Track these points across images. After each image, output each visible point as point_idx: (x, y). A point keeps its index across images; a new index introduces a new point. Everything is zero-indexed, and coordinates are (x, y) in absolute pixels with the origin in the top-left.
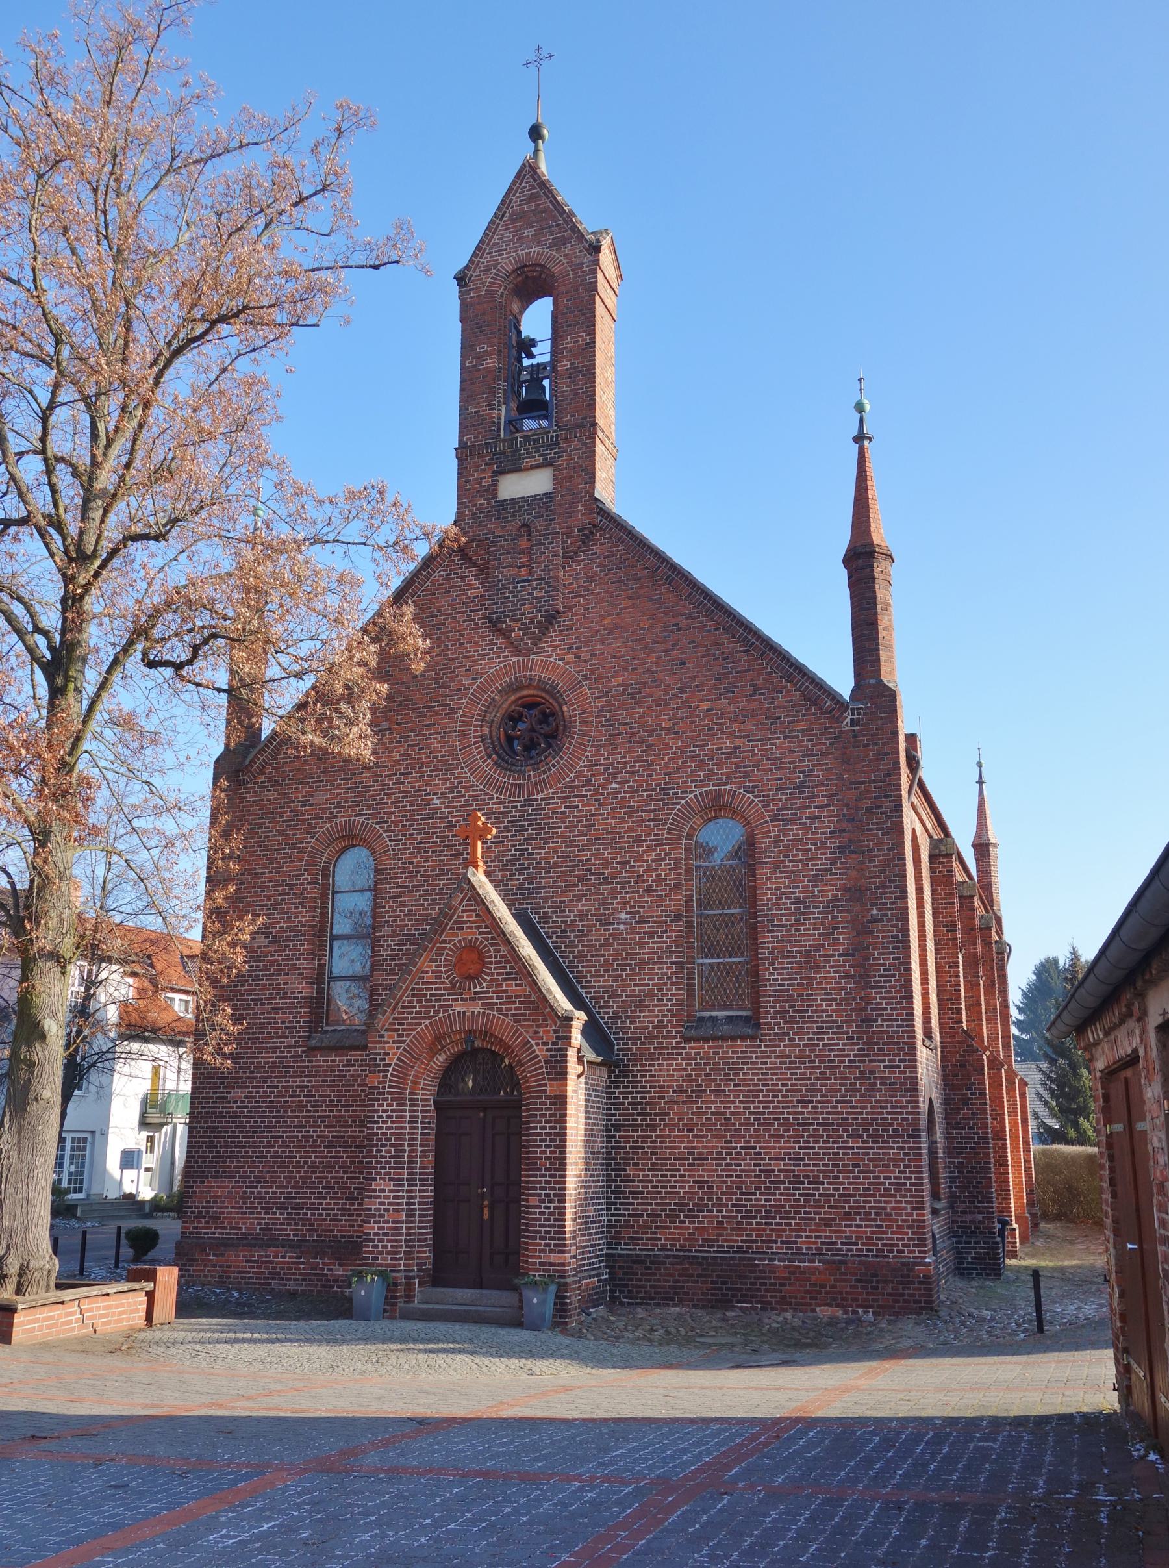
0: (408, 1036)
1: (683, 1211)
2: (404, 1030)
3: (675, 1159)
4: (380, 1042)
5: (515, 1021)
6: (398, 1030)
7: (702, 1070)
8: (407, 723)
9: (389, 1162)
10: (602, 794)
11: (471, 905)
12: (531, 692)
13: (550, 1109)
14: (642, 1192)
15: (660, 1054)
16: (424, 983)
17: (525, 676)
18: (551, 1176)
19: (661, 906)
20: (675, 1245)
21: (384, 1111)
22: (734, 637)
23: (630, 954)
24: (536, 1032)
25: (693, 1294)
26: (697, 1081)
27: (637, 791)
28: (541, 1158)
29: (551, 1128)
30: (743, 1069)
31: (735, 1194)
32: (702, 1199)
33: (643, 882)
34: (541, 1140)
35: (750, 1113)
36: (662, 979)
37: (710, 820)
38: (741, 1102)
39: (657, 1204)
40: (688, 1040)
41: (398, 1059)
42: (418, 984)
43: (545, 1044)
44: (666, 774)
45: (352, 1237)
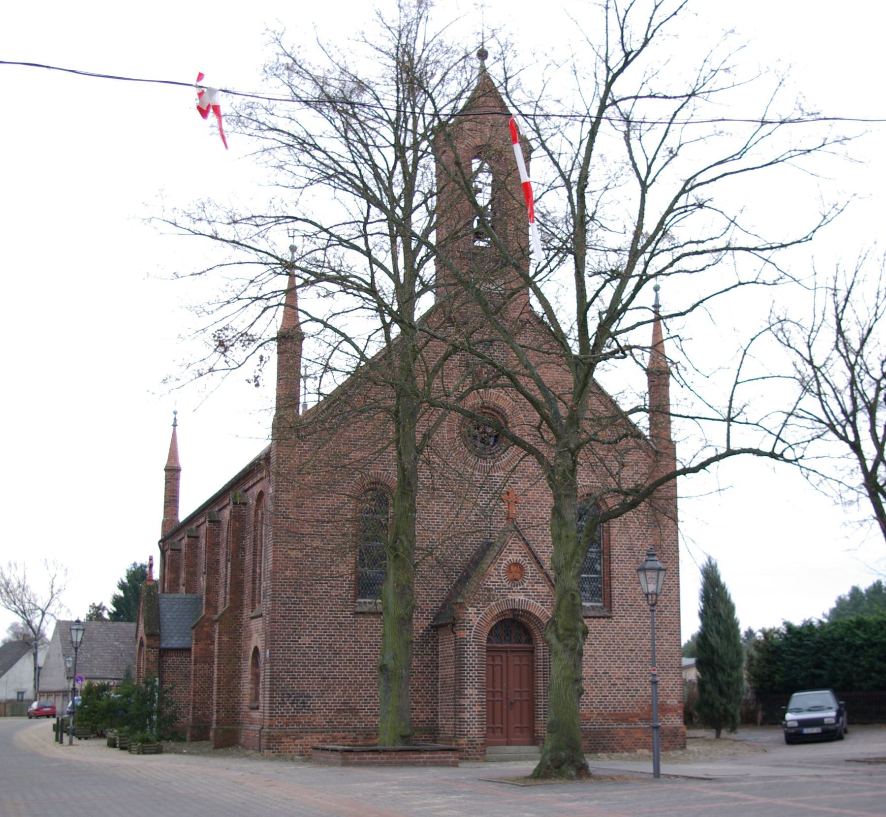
16: (491, 582)
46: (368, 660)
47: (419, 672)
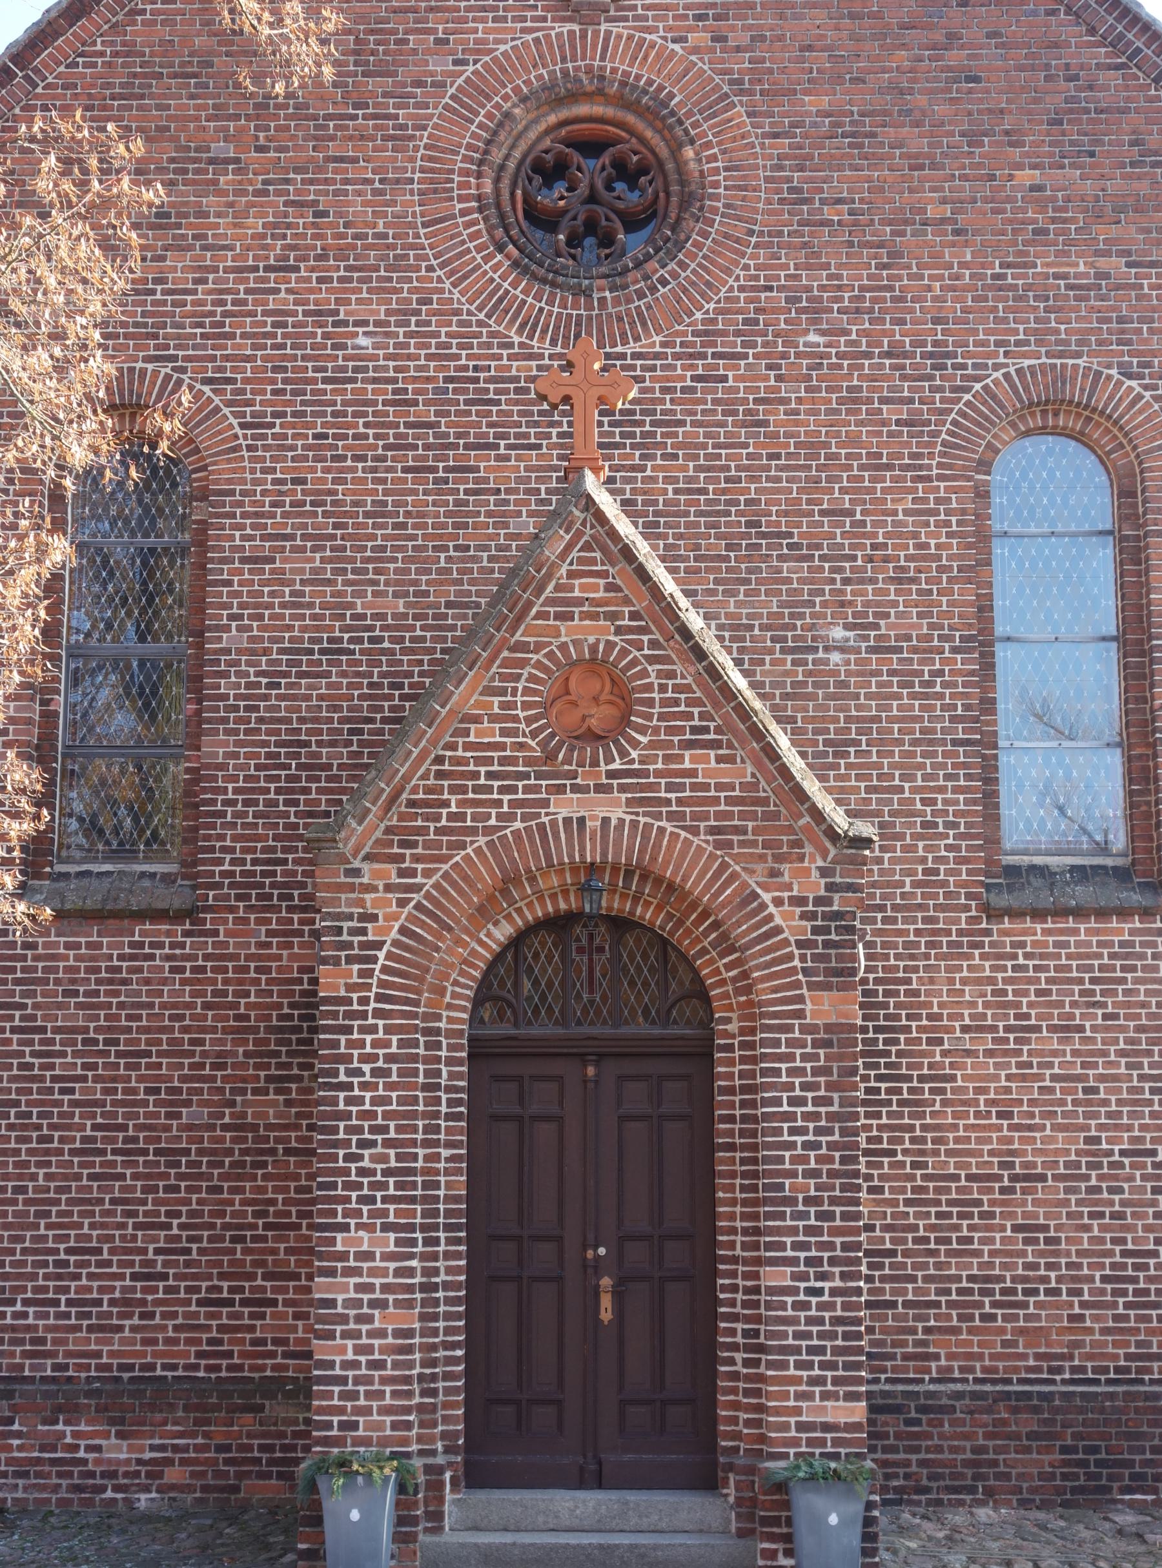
0: (427, 874)
1: (989, 1293)
2: (417, 859)
3: (969, 1178)
4: (351, 888)
5: (718, 845)
6: (400, 858)
7: (1030, 981)
8: (285, 149)
9: (384, 1186)
10: (784, 356)
11: (593, 562)
12: (598, 110)
13: (815, 1057)
14: (892, 1253)
15: (930, 945)
16: (468, 747)
17: (589, 70)
18: (820, 1216)
19: (930, 615)
20: (972, 1370)
21: (366, 1059)
22: (1092, 31)
23: (858, 719)
24: (774, 873)
25: (1020, 1476)
26: (1018, 1005)
27: (868, 355)
28: (793, 1174)
29: (817, 1101)
30: (1123, 981)
31: (1110, 1253)
32: (1034, 1266)
33: (886, 559)
34: (793, 1131)
35: (1142, 1078)
36: (932, 777)
37: (1028, 433)
38: (1121, 1053)
39: (927, 1279)
40: (993, 913)
41: (403, 931)
42: (452, 747)
43: (800, 901)
44: (936, 321)
45: (151, 1367)
46: (74, 1103)
47: (288, 1152)
